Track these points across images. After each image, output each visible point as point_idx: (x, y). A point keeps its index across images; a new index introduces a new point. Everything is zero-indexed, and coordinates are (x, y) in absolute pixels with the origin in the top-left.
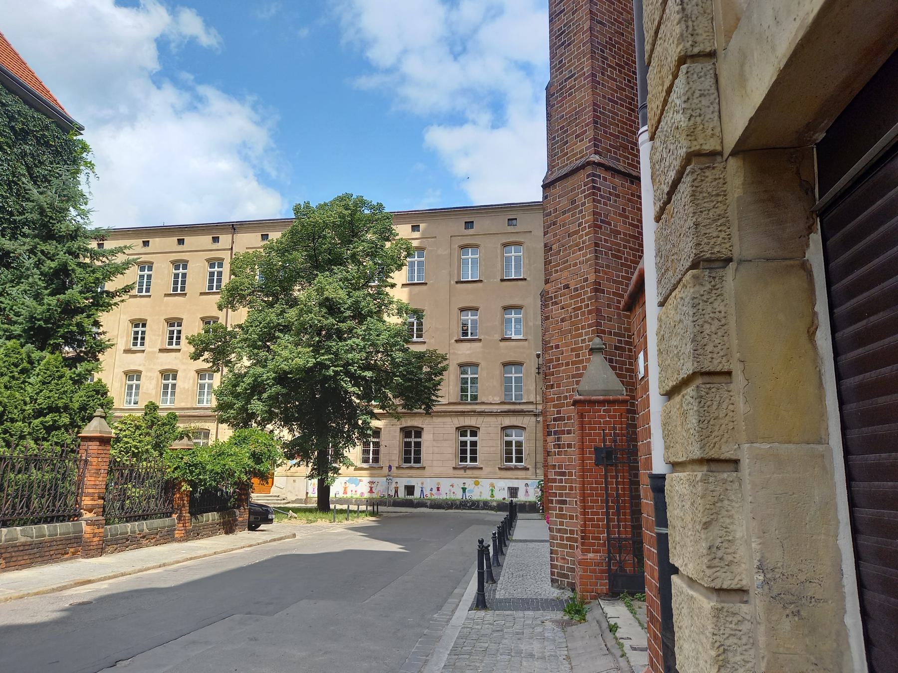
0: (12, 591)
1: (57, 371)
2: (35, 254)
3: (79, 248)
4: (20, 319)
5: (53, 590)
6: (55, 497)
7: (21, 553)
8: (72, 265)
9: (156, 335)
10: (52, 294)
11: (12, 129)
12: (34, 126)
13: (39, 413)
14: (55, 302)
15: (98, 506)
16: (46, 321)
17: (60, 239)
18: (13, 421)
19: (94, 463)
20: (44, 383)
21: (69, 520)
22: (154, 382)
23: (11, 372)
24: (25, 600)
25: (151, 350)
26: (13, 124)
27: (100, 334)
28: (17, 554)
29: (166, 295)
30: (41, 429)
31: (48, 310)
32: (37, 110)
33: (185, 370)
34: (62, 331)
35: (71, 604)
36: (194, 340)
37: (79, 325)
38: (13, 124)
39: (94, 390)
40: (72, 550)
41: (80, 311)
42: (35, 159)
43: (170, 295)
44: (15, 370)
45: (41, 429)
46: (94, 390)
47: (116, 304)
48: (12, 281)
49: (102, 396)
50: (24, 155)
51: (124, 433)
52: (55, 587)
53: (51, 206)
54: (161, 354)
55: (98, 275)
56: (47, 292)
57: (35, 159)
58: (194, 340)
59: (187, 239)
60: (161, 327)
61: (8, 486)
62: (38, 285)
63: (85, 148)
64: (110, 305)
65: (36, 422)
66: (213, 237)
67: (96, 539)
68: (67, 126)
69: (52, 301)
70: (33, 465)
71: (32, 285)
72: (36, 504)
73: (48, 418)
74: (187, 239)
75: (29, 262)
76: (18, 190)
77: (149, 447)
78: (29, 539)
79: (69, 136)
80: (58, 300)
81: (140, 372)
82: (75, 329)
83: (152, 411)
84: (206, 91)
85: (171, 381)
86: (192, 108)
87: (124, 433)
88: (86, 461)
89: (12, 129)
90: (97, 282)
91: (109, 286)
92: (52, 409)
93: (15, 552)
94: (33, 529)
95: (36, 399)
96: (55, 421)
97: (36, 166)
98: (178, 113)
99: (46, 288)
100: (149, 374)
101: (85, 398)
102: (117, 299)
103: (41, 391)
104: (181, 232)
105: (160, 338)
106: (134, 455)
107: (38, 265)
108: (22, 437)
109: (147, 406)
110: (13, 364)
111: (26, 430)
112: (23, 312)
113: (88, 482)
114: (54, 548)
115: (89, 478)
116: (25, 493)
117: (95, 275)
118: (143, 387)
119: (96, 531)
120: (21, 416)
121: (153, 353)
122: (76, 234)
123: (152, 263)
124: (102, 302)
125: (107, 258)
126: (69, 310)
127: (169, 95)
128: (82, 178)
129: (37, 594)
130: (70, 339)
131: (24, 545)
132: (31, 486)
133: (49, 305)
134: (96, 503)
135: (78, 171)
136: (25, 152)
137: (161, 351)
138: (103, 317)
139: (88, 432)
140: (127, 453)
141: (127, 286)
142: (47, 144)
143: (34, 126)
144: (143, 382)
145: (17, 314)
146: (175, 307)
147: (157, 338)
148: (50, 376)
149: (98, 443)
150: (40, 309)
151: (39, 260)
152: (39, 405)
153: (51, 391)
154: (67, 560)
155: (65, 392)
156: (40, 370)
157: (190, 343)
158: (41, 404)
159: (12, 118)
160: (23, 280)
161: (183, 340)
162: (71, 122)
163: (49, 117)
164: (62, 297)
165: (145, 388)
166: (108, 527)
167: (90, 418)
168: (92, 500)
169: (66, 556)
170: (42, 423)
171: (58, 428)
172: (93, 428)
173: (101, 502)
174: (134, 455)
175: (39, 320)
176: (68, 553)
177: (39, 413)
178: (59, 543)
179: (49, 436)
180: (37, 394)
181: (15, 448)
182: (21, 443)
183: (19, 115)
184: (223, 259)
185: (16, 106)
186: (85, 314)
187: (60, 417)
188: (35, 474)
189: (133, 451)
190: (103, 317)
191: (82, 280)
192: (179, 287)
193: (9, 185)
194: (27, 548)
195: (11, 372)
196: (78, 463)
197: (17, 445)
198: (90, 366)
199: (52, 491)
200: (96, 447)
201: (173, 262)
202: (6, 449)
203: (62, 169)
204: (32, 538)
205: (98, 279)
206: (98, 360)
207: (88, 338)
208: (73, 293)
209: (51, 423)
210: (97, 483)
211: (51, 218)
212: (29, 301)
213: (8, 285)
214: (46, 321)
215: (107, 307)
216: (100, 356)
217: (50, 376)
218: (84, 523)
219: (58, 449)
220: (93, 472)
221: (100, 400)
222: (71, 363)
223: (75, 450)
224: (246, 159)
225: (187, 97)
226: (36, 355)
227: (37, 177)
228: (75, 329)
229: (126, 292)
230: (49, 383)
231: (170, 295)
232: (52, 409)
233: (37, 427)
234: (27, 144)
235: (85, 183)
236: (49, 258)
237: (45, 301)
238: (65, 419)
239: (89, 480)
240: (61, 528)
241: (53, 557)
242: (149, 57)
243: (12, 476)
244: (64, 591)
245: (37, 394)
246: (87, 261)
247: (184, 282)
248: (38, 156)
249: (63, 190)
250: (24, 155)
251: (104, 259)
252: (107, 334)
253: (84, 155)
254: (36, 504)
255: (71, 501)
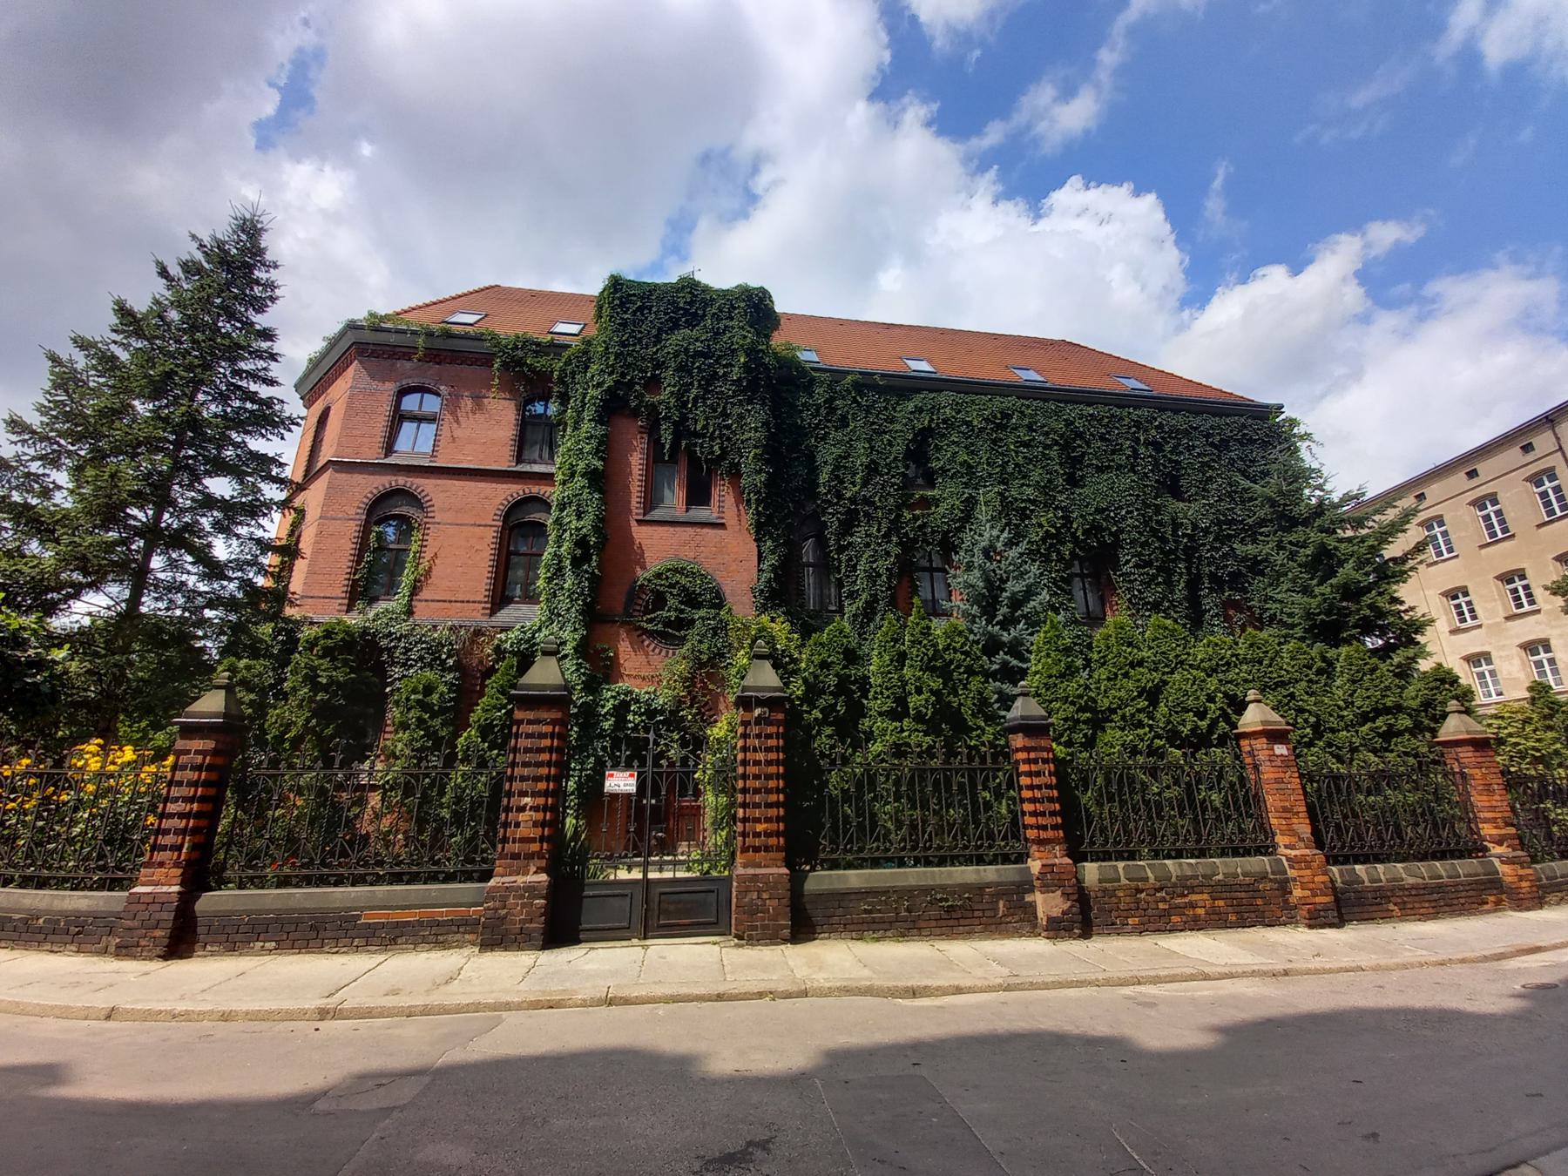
0: (1424, 952)
1: (1366, 664)
2: (1284, 548)
3: (1332, 522)
4: (1296, 620)
5: (1486, 959)
6: (1435, 825)
7: (1416, 899)
8: (1331, 542)
9: (1490, 602)
10: (1320, 584)
11: (1212, 445)
12: (1231, 431)
13: (1365, 718)
14: (1329, 589)
15: (1512, 837)
16: (1328, 613)
17: (1306, 522)
18: (1333, 731)
19: (1477, 777)
20: (1354, 682)
21: (1470, 857)
22: (1516, 662)
23: (1306, 676)
24: (1448, 970)
25: (1489, 622)
26: (1210, 440)
27: (1406, 611)
28: (1411, 899)
29: (1482, 547)
30: (1374, 737)
31: (1325, 600)
32: (1228, 416)
33: (1561, 636)
34: (1352, 620)
35: (1524, 986)
36: (1559, 588)
37: (1372, 607)
38: (1210, 440)
39: (1436, 680)
40: (1492, 898)
41: (1368, 589)
42: (1245, 462)
43: (1489, 544)
44: (1310, 672)
45: (1374, 737)
46: (1436, 680)
47: (1412, 569)
48: (1271, 585)
49: (1452, 685)
50: (1232, 462)
51: (1506, 731)
52: (1486, 953)
53: (1280, 493)
54: (1510, 624)
55: (1370, 542)
56: (1314, 582)
57: (1245, 462)
58: (1559, 588)
59: (1480, 467)
60: (1494, 589)
61: (1362, 812)
62: (1300, 578)
63: (1293, 423)
64: (1405, 572)
65: (1365, 728)
66: (1521, 448)
67: (1524, 884)
68: (1263, 413)
69: (1325, 589)
70: (1384, 784)
71: (1294, 581)
72: (1410, 834)
73: (1379, 722)
74: (1480, 467)
75: (1280, 558)
76: (1240, 497)
77: (1558, 746)
78: (1420, 881)
79: (1270, 422)
80: (1331, 586)
81: (1489, 653)
82: (1368, 612)
83: (1543, 694)
84: (1434, 287)
85: (1484, 667)
86: (1422, 318)
87: (1506, 731)
88: (1463, 775)
89: (1212, 445)
90: (1375, 550)
91: (1392, 551)
92: (1378, 712)
93: (1406, 896)
94: (1423, 867)
95: (1353, 703)
96: (1391, 726)
97: (1249, 467)
98: (1406, 336)
99: (1312, 579)
100: (1503, 654)
101: (1426, 692)
102: (1411, 563)
103: (1355, 691)
104: (1468, 463)
105: (1499, 603)
106: (1536, 761)
107: (1292, 556)
108: (1354, 750)
109: (1530, 689)
110: (1304, 666)
111: (1357, 741)
112: (1297, 611)
113: (1479, 804)
114: (1463, 894)
115: (1479, 798)
116: (1388, 818)
117: (1366, 544)
118: (1501, 672)
119: (1521, 872)
120: (1342, 724)
121: (1498, 624)
122: (1320, 509)
123: (1441, 516)
124: (1392, 572)
125: (1374, 521)
126: (1352, 592)
127: (1388, 321)
128: (1304, 454)
129: (1463, 961)
130: (1367, 627)
131: (1414, 887)
132: (1394, 813)
133: (1324, 594)
134: (1503, 832)
135: (1297, 450)
136: (1233, 459)
137: (1507, 618)
138: (1404, 591)
139: (1447, 734)
140: (1523, 758)
141: (1418, 543)
142: (1252, 441)
143: (1231, 431)
144: (1497, 664)
145: (1291, 615)
146: (1505, 556)
147: (1494, 604)
148: (1358, 672)
149: (1471, 748)
150: (1314, 602)
151: (1291, 553)
152: (1358, 708)
153: (1367, 690)
154: (1488, 912)
155: (1388, 688)
156: (1341, 667)
157: (1555, 594)
158: (1361, 707)
159: (1208, 436)
160: (1282, 579)
161: (1539, 593)
162: (1267, 406)
163: (1242, 416)
164: (1334, 581)
165: (1505, 673)
166: (1538, 866)
167: (1444, 716)
168: (1496, 828)
169: (1486, 907)
170: (1371, 729)
171: (1400, 734)
172: (1453, 727)
173: (1512, 830)
174: (1536, 761)
175: (1319, 614)
176: (1487, 903)
177: (1365, 718)
178: (1468, 888)
179: (1390, 746)
180: (1351, 695)
181: (1351, 763)
182: (1355, 756)
183: (1213, 429)
184: (1553, 468)
185: (1205, 422)
186: (1374, 592)
187: (1396, 719)
188: (1394, 797)
189: (1533, 755)
190: (1404, 591)
191: (1351, 556)
192: (1498, 531)
193: (1230, 496)
194: (1422, 892)
195: (1306, 676)
196: (1451, 777)
197: (1352, 760)
198: (1411, 652)
199: (1424, 814)
200: (1470, 754)
201: (1473, 503)
202: (1339, 766)
203: (1274, 453)
204: (1423, 878)
205: (1372, 547)
206: (1418, 643)
207: (1392, 619)
208: (1347, 571)
209: (1384, 728)
210: (1494, 803)
211: (1285, 505)
212: (1297, 597)
213: (1268, 590)
214: (1328, 613)
215: (1401, 576)
216: (1419, 638)
217: (1358, 672)
218: (1497, 862)
219: (1411, 760)
220: (1480, 788)
221: (1451, 691)
222: (1384, 653)
223: (1439, 761)
224: (1540, 330)
225: (1413, 310)
226: (1332, 653)
227: (1254, 476)
228: (1368, 612)
229: (1420, 551)
230: (1361, 679)
231: (1489, 544)
232: (1378, 712)
233: (1367, 735)
234: (1231, 451)
235: (1308, 456)
236: (1301, 547)
237: (1317, 590)
238: (1405, 722)
239: (1479, 800)
240: (1464, 867)
241: (1467, 906)
242: (1353, 295)
243: (1362, 798)
244: (1504, 962)
245: (1351, 695)
246: (1349, 533)
247: (1502, 522)
248: (1247, 456)
249: (1286, 471)
250: (1232, 462)
251: (1371, 524)
252: (1417, 610)
253: (1295, 431)
254: (1410, 834)
255: (1461, 828)
